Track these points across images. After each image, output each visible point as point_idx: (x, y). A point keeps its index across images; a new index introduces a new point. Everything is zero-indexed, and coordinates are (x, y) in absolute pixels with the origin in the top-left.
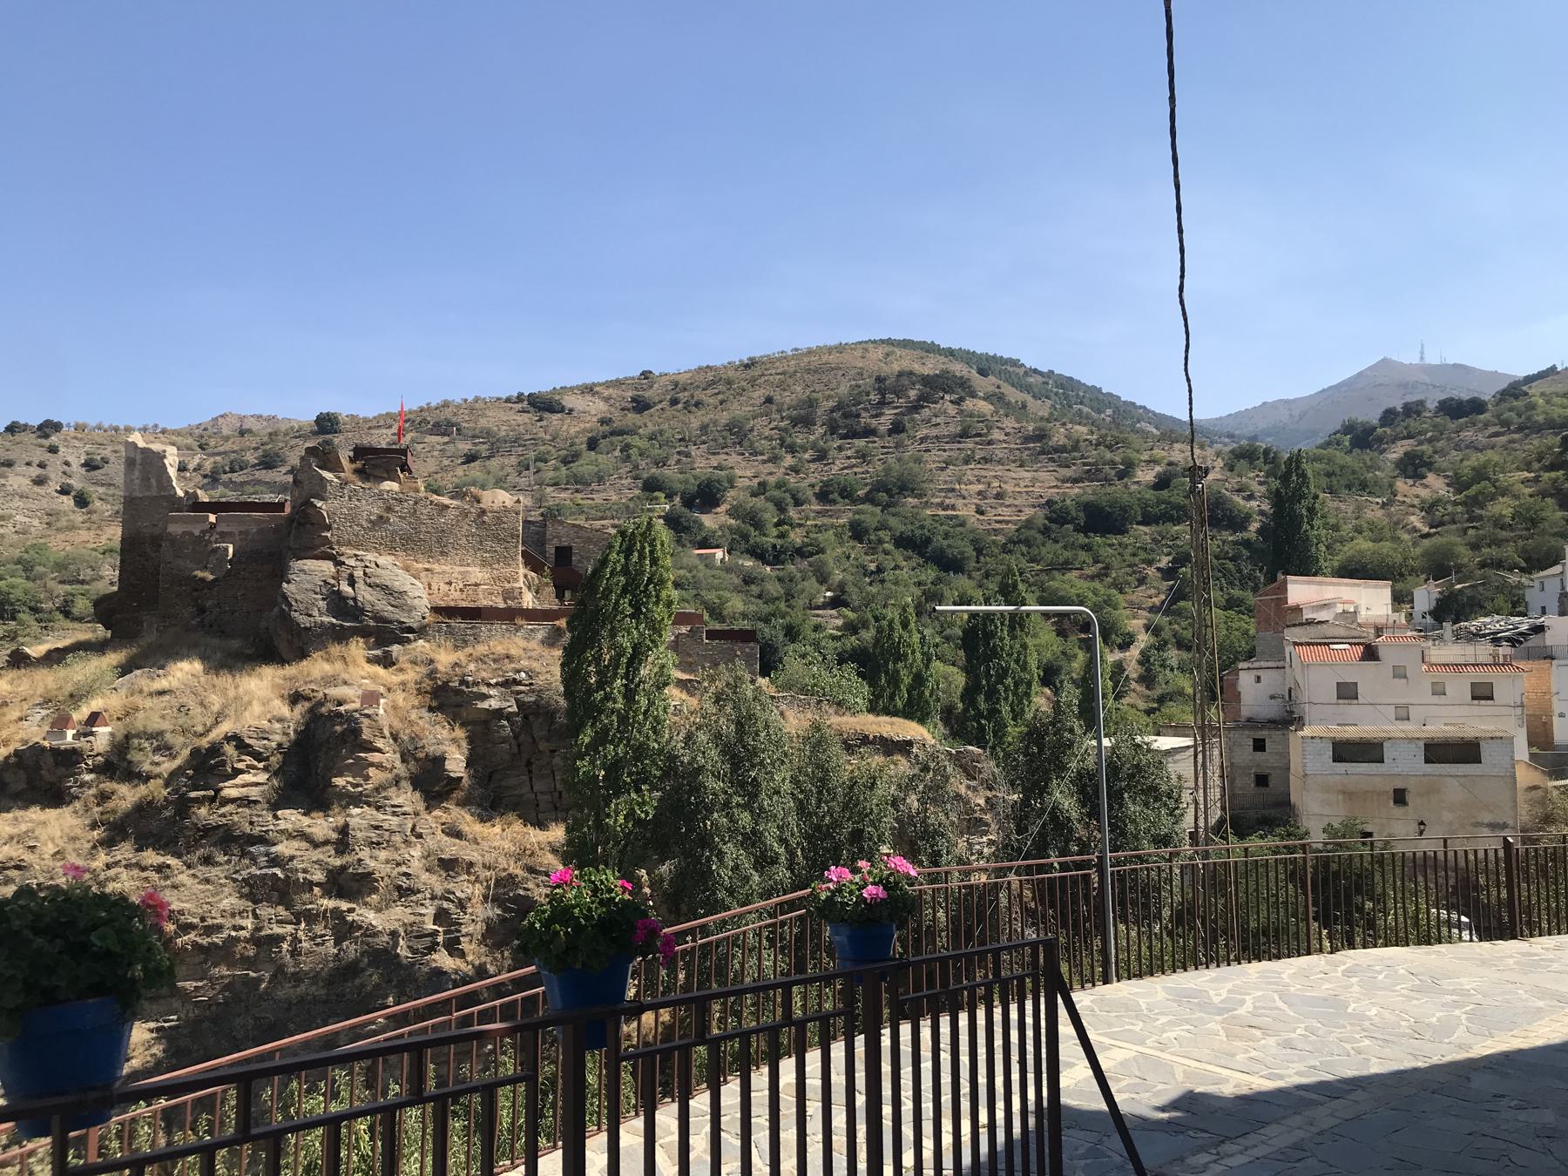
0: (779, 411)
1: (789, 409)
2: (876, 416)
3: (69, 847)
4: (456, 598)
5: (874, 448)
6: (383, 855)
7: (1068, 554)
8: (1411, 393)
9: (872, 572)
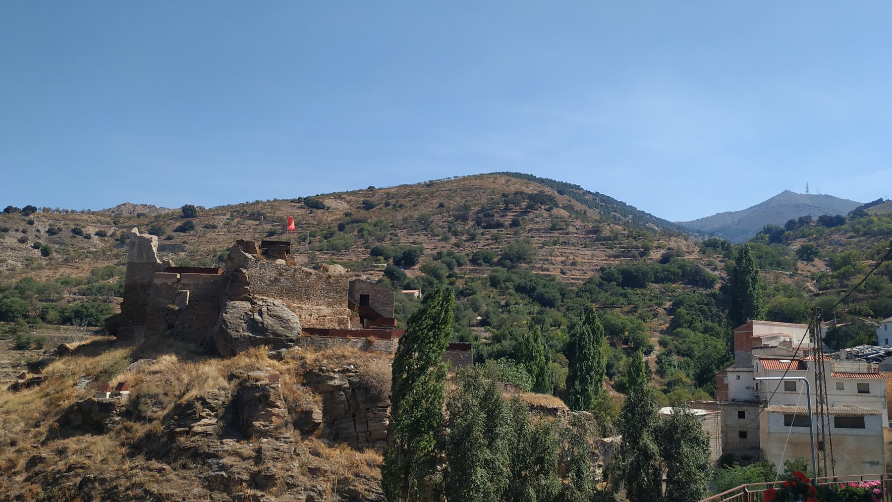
0: (448, 212)
1: (453, 211)
2: (503, 216)
3: (110, 457)
4: (313, 323)
6: (279, 465)
7: (613, 299)
8: (801, 211)
9: (503, 306)
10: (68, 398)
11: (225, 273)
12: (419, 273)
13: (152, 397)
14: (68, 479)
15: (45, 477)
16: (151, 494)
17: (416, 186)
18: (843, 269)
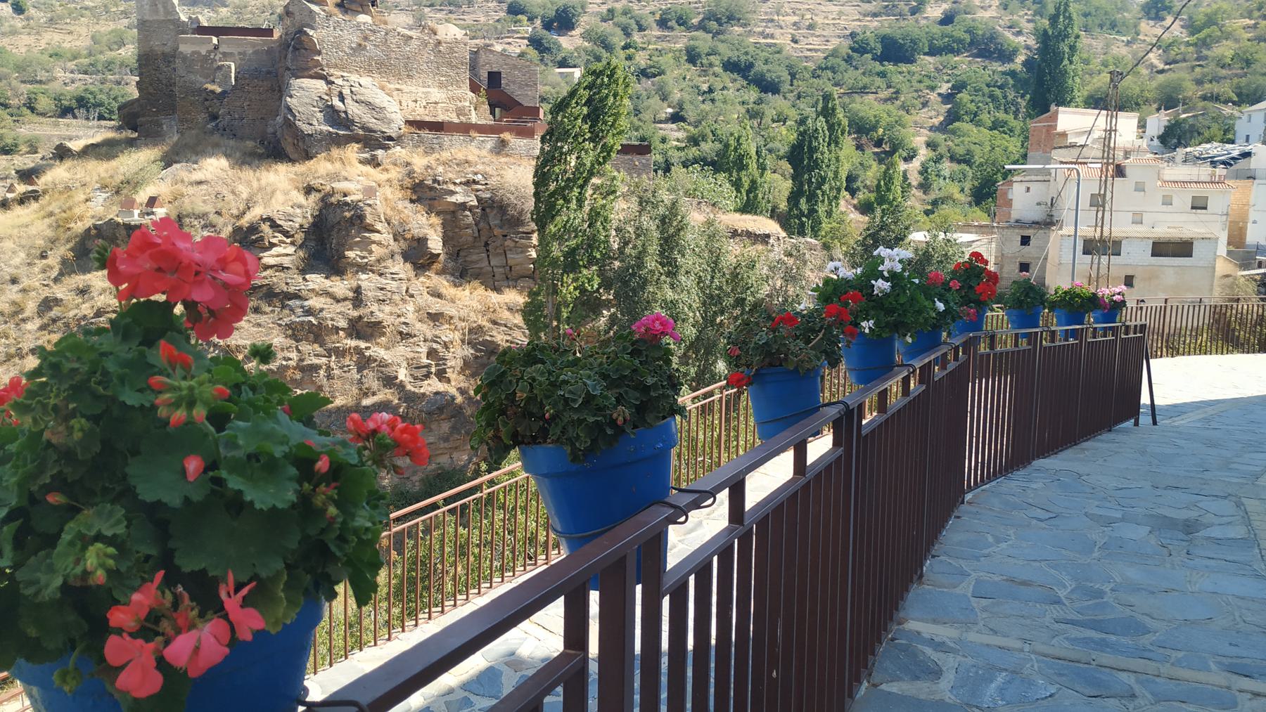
6: (387, 309)
7: (866, 80)
9: (705, 92)
10: (81, 218)
11: (283, 36)
12: (578, 41)
13: (200, 217)
18: (1206, 32)
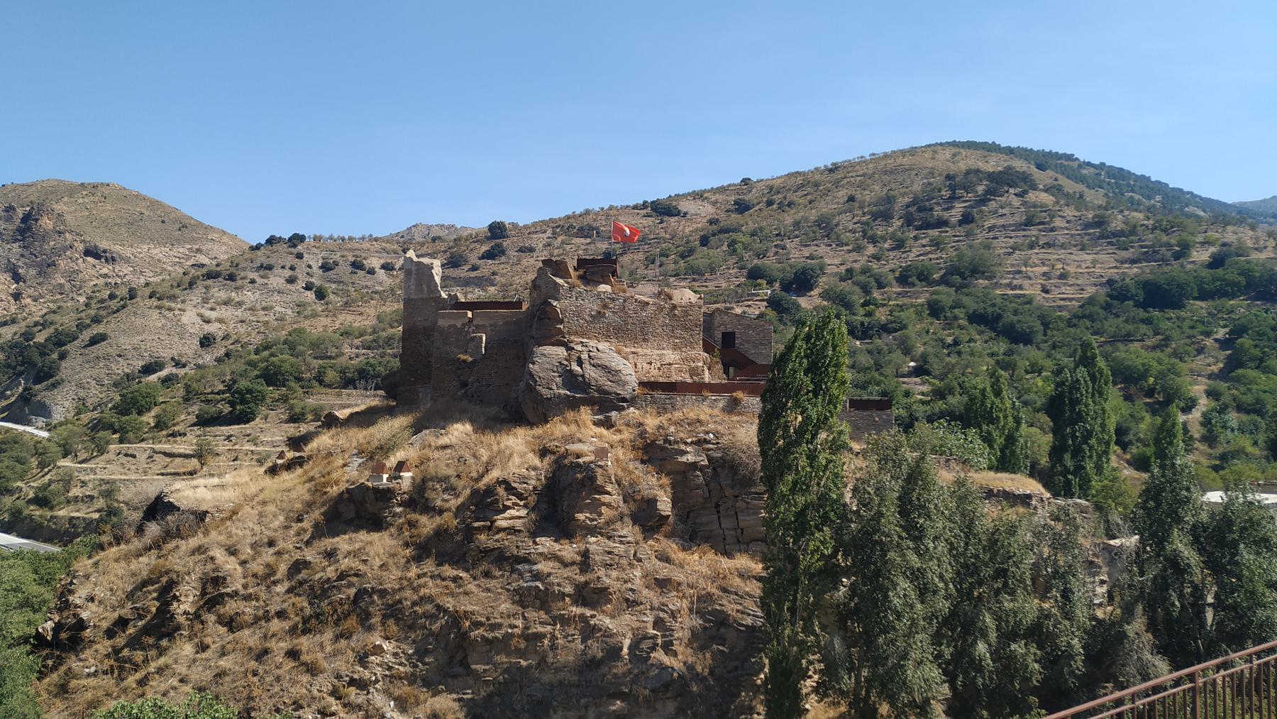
0: (861, 207)
1: (869, 206)
2: (948, 209)
3: (391, 561)
4: (655, 374)
5: (946, 236)
6: (614, 574)
7: (1129, 327)
9: (950, 345)
10: (337, 482)
12: (818, 301)
13: (442, 481)
14: (340, 590)
15: (312, 588)
16: (446, 611)
17: (812, 172)
